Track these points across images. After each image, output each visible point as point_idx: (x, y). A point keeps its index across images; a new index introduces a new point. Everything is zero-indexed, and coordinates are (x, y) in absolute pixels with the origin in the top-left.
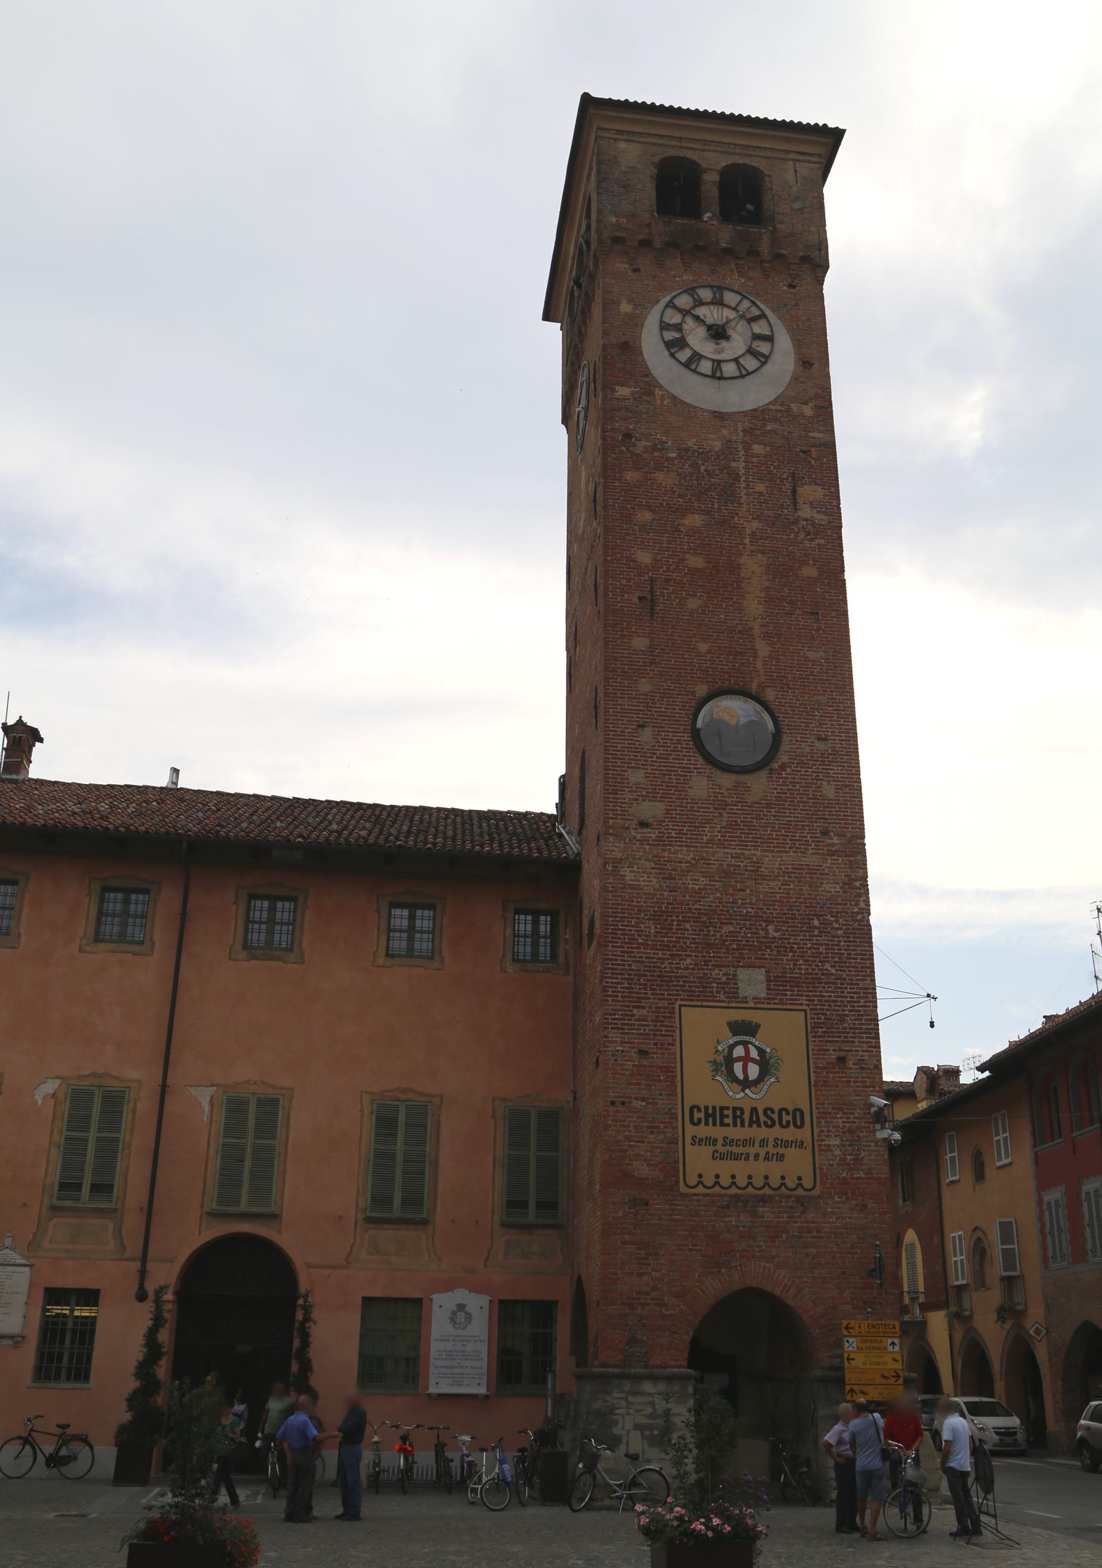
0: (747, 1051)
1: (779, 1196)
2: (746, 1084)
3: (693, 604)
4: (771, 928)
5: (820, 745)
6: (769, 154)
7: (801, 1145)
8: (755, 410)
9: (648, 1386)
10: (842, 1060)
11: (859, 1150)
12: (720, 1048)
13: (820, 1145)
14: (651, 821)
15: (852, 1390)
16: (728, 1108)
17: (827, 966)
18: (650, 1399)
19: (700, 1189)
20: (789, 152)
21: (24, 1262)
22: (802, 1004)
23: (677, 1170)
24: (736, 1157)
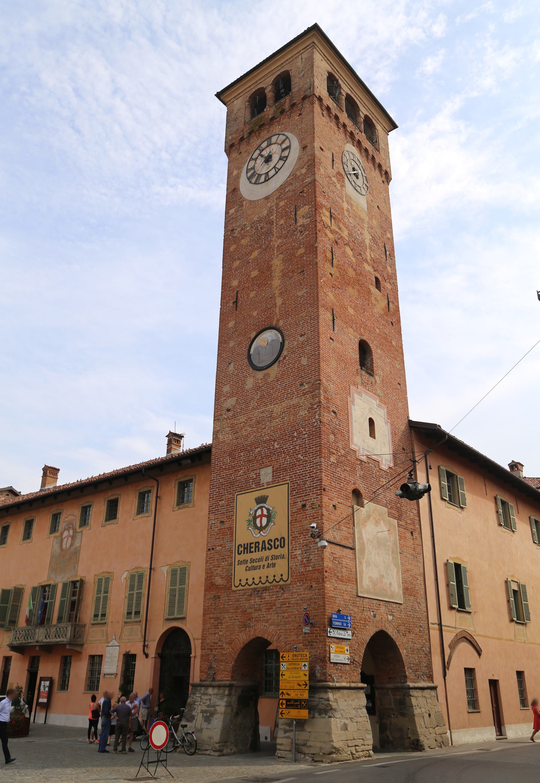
0: (262, 511)
1: (273, 586)
2: (261, 529)
3: (252, 294)
4: (275, 444)
5: (301, 339)
6: (292, 59)
7: (283, 557)
8: (281, 186)
9: (210, 691)
10: (304, 506)
11: (310, 555)
12: (251, 513)
13: (291, 555)
14: (231, 408)
15: (282, 693)
16: (253, 543)
17: (299, 456)
18: (209, 697)
19: (240, 588)
20: (300, 52)
21: (117, 644)
22: (287, 480)
23: (231, 578)
24: (254, 568)
